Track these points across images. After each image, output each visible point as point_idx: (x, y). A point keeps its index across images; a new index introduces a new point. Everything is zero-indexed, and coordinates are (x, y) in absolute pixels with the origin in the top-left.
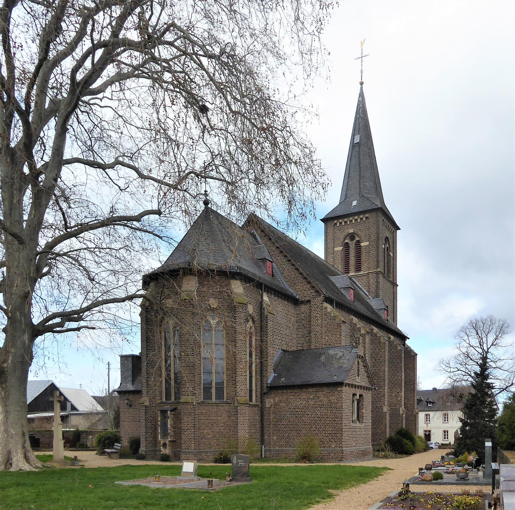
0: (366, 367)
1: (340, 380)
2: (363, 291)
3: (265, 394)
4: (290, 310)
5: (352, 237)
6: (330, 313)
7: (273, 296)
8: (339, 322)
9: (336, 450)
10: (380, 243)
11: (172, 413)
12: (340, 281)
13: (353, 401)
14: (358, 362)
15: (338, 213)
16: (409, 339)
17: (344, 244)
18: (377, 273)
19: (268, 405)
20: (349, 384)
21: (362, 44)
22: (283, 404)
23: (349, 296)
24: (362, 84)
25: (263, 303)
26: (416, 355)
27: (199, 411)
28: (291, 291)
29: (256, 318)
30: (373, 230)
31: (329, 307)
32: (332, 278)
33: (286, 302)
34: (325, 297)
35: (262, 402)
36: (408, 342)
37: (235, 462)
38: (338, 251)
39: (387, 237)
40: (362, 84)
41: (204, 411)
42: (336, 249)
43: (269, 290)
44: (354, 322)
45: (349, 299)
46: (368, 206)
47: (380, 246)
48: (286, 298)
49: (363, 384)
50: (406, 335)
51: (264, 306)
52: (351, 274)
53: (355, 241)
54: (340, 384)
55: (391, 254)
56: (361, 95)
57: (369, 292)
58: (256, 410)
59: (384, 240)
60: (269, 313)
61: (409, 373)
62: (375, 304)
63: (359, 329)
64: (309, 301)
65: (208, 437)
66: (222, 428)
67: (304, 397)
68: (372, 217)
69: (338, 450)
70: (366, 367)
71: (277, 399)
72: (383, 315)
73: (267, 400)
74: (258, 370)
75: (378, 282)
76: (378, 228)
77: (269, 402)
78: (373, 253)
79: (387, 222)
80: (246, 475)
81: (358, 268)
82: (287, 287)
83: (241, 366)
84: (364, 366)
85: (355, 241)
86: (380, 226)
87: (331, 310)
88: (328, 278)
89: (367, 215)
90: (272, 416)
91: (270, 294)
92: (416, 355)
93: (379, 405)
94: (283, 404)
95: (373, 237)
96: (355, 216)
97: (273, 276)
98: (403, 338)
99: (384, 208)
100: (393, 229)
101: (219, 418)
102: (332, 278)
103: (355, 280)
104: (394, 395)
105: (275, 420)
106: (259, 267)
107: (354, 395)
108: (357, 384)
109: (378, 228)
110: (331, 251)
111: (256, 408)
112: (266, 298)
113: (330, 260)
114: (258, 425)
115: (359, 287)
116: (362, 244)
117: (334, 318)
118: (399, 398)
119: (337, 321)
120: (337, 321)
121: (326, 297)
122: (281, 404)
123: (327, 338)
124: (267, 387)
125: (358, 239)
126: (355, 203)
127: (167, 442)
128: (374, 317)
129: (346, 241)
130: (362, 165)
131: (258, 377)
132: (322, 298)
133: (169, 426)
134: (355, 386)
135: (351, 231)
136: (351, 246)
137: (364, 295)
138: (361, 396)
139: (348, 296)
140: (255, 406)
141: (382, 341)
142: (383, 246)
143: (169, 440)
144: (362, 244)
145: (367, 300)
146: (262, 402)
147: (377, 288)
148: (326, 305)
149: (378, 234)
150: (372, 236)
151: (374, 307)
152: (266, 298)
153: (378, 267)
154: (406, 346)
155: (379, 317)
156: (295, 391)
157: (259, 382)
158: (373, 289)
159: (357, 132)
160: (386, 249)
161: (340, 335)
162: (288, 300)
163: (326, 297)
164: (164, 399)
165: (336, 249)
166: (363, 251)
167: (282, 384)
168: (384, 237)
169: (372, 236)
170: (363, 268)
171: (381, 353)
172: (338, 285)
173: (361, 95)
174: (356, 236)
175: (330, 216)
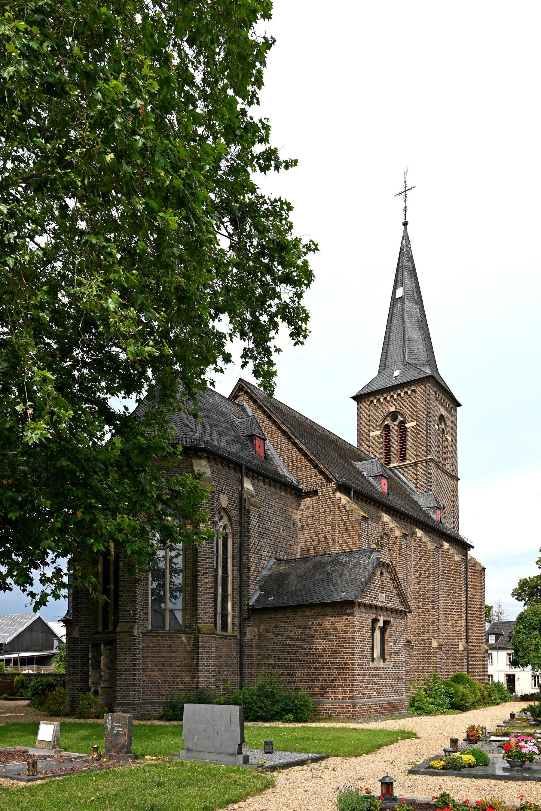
1: (350, 598)
3: (245, 619)
5: (394, 416)
6: (345, 506)
7: (261, 484)
8: (358, 518)
9: (344, 703)
10: (432, 422)
11: (107, 647)
13: (373, 630)
14: (381, 573)
15: (375, 388)
16: (473, 547)
18: (426, 461)
19: (248, 636)
20: (365, 605)
21: (405, 174)
22: (271, 634)
23: (382, 486)
24: (405, 224)
25: (244, 492)
26: (484, 569)
27: (144, 645)
29: (234, 513)
30: (422, 405)
31: (344, 499)
32: (357, 464)
33: (283, 494)
35: (242, 632)
36: (471, 553)
37: (110, 727)
38: (375, 436)
39: (442, 415)
40: (405, 224)
41: (151, 645)
42: (372, 434)
43: (255, 475)
45: (380, 490)
46: (415, 375)
47: (432, 426)
48: (272, 483)
49: (390, 605)
50: (468, 542)
51: (245, 496)
53: (397, 422)
54: (351, 604)
55: (449, 438)
56: (406, 238)
57: (417, 487)
58: (234, 644)
59: (437, 419)
60: (252, 505)
61: (474, 594)
65: (157, 682)
66: (178, 669)
67: (299, 623)
69: (347, 702)
70: (395, 580)
71: (262, 627)
73: (248, 629)
74: (236, 586)
75: (428, 473)
77: (251, 632)
78: (422, 435)
80: (125, 749)
81: (403, 458)
82: (286, 473)
83: (206, 580)
84: (391, 579)
85: (397, 422)
86: (432, 400)
88: (351, 464)
89: (413, 388)
90: (255, 652)
91: (256, 481)
92: (484, 569)
93: (426, 638)
94: (271, 634)
95: (422, 415)
97: (265, 458)
98: (464, 546)
99: (437, 378)
100: (451, 405)
101: (173, 654)
102: (357, 464)
104: (450, 624)
105: (260, 657)
106: (244, 446)
107: (375, 621)
108: (379, 604)
109: (428, 403)
110: (366, 436)
111: (233, 640)
112: (248, 485)
114: (236, 666)
116: (407, 425)
117: (351, 512)
118: (458, 629)
120: (355, 516)
121: (338, 485)
122: (267, 634)
123: (341, 542)
124: (248, 610)
125: (401, 419)
127: (99, 689)
128: (421, 517)
129: (386, 423)
131: (237, 596)
132: (333, 485)
133: (102, 667)
134: (376, 607)
135: (392, 409)
136: (391, 428)
138: (386, 622)
139: (378, 487)
140: (230, 637)
142: (437, 427)
143: (102, 686)
144: (407, 425)
146: (242, 632)
147: (428, 481)
148: (338, 495)
151: (422, 506)
152: (248, 485)
153: (428, 452)
154: (469, 558)
155: (429, 517)
156: (288, 615)
157: (238, 603)
158: (422, 483)
159: (399, 284)
160: (441, 431)
161: (360, 536)
162: (286, 491)
164: (100, 628)
165: (372, 434)
166: (409, 434)
168: (438, 415)
169: (421, 414)
170: (409, 456)
172: (365, 474)
173: (406, 238)
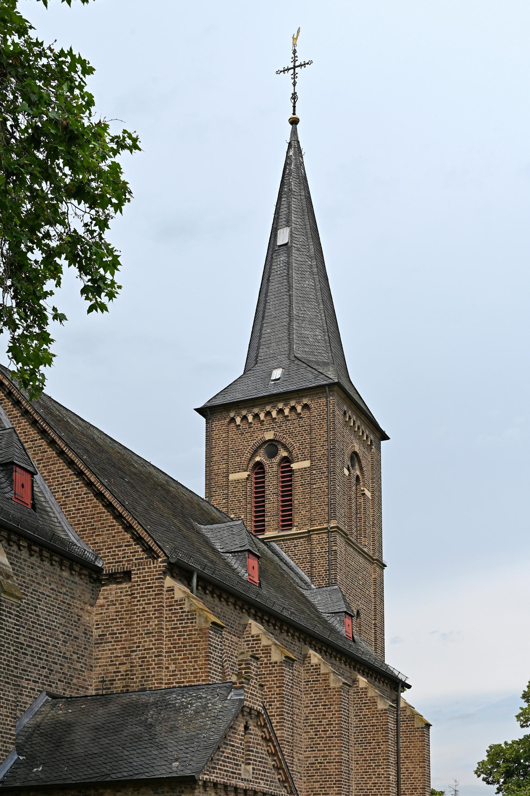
0: (270, 740)
1: (188, 773)
2: (296, 574)
4: (77, 594)
5: (272, 448)
8: (204, 625)
12: (225, 538)
15: (238, 396)
17: (251, 465)
18: (328, 531)
23: (247, 571)
28: (83, 546)
30: (320, 434)
31: (180, 590)
33: (65, 574)
34: (167, 561)
38: (238, 481)
39: (355, 453)
40: (294, 122)
44: (253, 633)
52: (268, 534)
53: (277, 459)
56: (294, 145)
57: (311, 576)
62: (324, 601)
63: (267, 650)
64: (127, 575)
68: (318, 405)
70: (270, 740)
72: (343, 628)
75: (332, 552)
76: (331, 429)
79: (354, 417)
81: (287, 522)
85: (277, 459)
87: (182, 595)
89: (305, 401)
91: (15, 548)
95: (320, 451)
96: (279, 401)
97: (34, 506)
98: (395, 684)
102: (204, 529)
103: (277, 548)
109: (331, 429)
113: (218, 501)
115: (286, 564)
116: (295, 466)
117: (192, 615)
119: (200, 623)
120: (200, 623)
121: (170, 563)
123: (172, 667)
125: (285, 454)
126: (277, 374)
128: (319, 630)
129: (258, 459)
130: (294, 293)
132: (160, 564)
135: (269, 436)
136: (267, 468)
137: (298, 580)
139: (242, 571)
141: (332, 685)
142: (346, 472)
144: (295, 466)
145: (304, 592)
147: (331, 565)
148: (169, 582)
149: (331, 443)
150: (319, 447)
153: (332, 516)
155: (333, 630)
158: (320, 569)
160: (353, 480)
163: (170, 563)
166: (297, 481)
167: (34, 783)
169: (319, 447)
170: (297, 519)
171: (329, 715)
173: (294, 145)
174: (279, 447)
175: (218, 402)
